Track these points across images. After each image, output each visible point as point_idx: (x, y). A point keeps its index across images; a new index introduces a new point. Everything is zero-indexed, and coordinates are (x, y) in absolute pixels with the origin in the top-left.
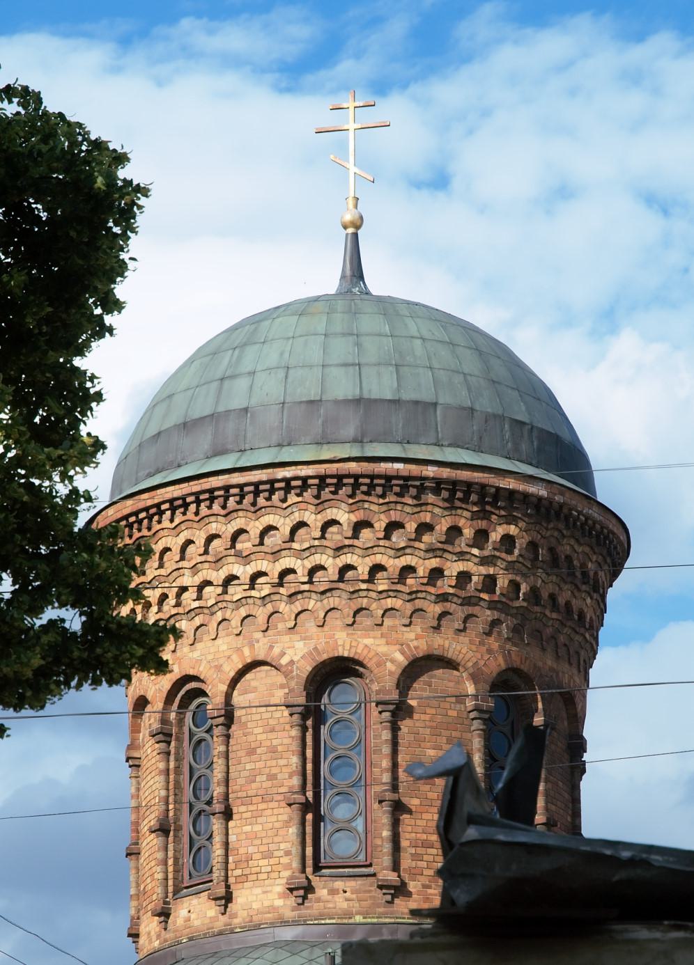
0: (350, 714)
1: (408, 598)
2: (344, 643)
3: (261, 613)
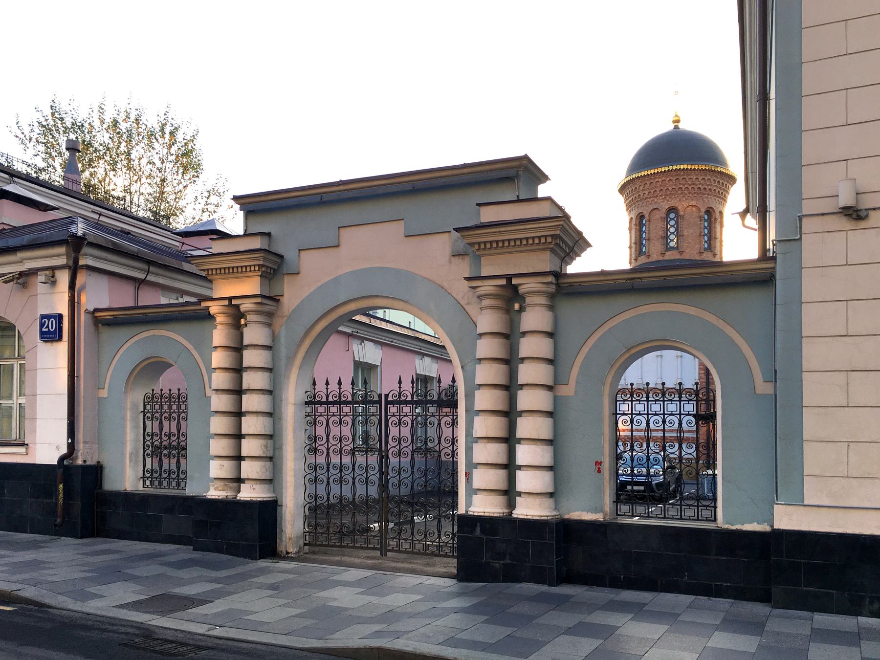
0: (171, 565)
3: (637, 205)
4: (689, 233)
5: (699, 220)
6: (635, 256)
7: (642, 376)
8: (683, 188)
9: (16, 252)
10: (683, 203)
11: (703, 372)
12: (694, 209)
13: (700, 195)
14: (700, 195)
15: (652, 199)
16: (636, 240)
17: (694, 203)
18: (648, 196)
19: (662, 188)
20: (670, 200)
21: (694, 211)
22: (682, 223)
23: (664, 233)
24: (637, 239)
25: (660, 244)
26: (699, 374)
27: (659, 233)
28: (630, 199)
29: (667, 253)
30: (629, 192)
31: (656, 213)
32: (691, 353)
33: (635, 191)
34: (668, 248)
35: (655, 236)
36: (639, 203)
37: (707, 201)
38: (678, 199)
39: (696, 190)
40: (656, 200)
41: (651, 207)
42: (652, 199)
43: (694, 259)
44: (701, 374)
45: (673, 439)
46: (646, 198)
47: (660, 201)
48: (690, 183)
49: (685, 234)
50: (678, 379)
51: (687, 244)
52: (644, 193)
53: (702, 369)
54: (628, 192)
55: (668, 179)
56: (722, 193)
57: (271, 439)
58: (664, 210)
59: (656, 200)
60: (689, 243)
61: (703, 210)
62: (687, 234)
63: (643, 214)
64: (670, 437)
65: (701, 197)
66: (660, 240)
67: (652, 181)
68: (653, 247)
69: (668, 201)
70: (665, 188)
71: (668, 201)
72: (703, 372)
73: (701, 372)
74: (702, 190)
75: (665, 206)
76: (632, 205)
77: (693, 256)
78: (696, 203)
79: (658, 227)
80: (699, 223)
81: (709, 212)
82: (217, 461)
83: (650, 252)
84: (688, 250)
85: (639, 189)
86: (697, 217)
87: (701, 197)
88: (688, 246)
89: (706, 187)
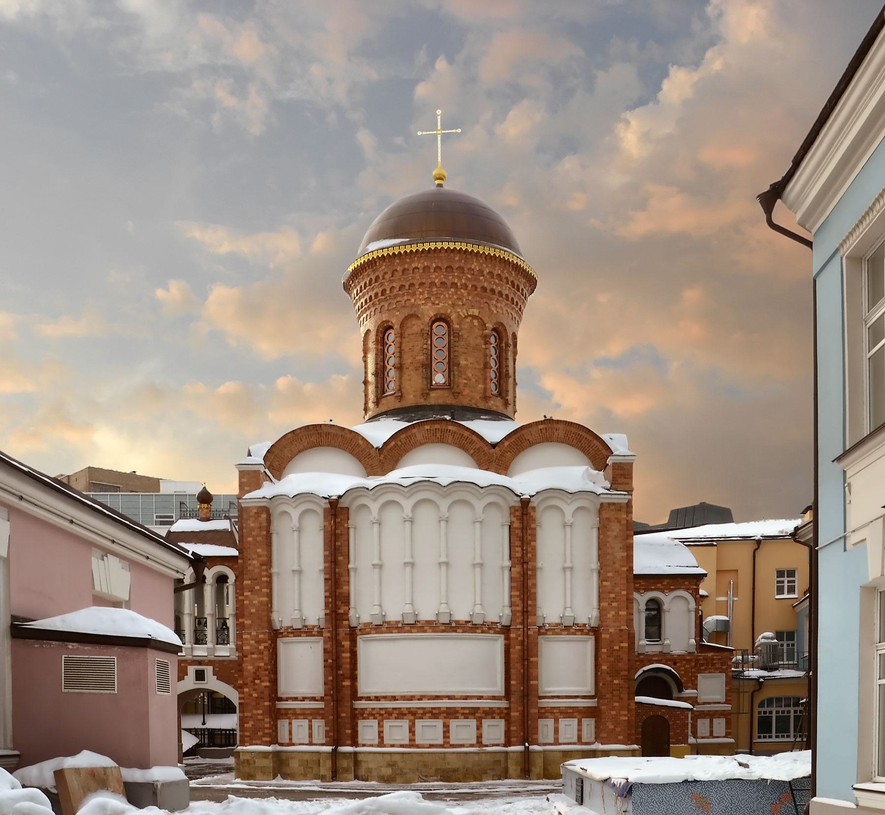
3: (378, 307)
4: (469, 363)
5: (483, 342)
6: (376, 396)
7: (412, 600)
8: (459, 284)
9: (357, 761)
10: (459, 310)
11: (518, 593)
12: (476, 322)
13: (485, 300)
14: (485, 300)
15: (406, 298)
16: (376, 368)
17: (476, 312)
18: (400, 292)
19: (424, 281)
20: (437, 302)
21: (475, 326)
22: (456, 344)
23: (427, 359)
24: (379, 367)
25: (420, 377)
26: (511, 597)
27: (418, 358)
28: (367, 297)
29: (433, 394)
30: (365, 284)
31: (413, 323)
32: (653, 530)
33: (365, 288)
34: (430, 387)
35: (412, 363)
36: (382, 304)
37: (495, 312)
38: (450, 303)
39: (479, 290)
40: (413, 300)
41: (406, 312)
42: (406, 298)
43: (475, 406)
44: (514, 596)
45: (467, 711)
46: (396, 296)
47: (419, 303)
48: (469, 276)
49: (461, 362)
50: (475, 605)
51: (466, 381)
52: (393, 287)
53: (514, 587)
54: (362, 284)
55: (434, 265)
56: (517, 302)
57: (622, 540)
58: (427, 319)
59: (413, 300)
60: (468, 379)
61: (490, 326)
62: (465, 363)
63: (390, 324)
64: (463, 708)
65: (486, 302)
66: (421, 369)
67: (406, 266)
68: (408, 382)
69: (433, 304)
70: (429, 281)
71: (433, 304)
72: (518, 593)
73: (513, 593)
74: (488, 291)
75: (429, 311)
76: (369, 308)
77: (473, 401)
78: (479, 312)
79: (418, 348)
80: (483, 346)
81: (499, 331)
83: (403, 390)
84: (466, 391)
85: (383, 278)
86: (481, 336)
87: (486, 302)
88: (465, 384)
89: (495, 287)
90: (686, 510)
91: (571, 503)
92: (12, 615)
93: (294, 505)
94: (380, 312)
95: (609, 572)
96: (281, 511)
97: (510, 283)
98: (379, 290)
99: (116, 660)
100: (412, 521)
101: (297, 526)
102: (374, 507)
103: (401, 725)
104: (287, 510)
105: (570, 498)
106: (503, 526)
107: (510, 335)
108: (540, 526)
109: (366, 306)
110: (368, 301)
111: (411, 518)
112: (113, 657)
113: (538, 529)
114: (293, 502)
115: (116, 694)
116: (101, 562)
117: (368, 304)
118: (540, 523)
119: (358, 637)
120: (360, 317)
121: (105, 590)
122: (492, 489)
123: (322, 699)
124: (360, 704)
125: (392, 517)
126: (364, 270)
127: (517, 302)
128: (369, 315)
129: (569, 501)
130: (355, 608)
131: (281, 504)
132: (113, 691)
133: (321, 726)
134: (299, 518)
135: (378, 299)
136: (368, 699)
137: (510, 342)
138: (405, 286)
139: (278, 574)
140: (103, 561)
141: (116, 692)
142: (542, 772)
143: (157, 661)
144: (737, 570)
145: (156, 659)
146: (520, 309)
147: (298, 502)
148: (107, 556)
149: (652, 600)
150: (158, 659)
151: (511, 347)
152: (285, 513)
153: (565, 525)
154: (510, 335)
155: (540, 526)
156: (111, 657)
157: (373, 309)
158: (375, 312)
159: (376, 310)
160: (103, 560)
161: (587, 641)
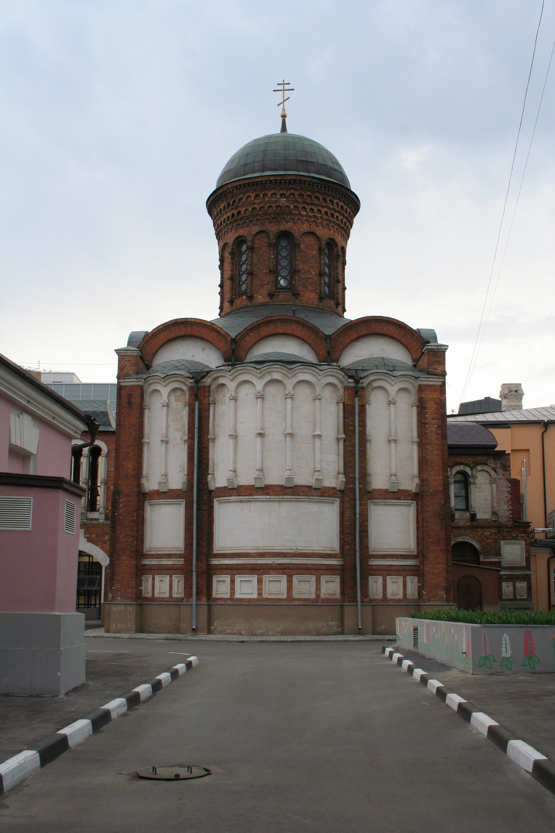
1: (258, 204)
2: (241, 232)
54: (222, 207)
82: (487, 733)
90: (467, 405)
91: (395, 384)
92: (115, 350)
93: (164, 384)
94: (235, 230)
95: (427, 445)
96: (153, 389)
97: (340, 208)
98: (235, 212)
99: (32, 500)
100: (262, 397)
101: (87, 454)
102: (231, 386)
103: (250, 580)
104: (158, 389)
105: (393, 380)
106: (338, 403)
107: (339, 249)
108: (369, 404)
109: (228, 222)
110: (226, 221)
111: (262, 395)
112: (30, 498)
113: (367, 406)
114: (164, 382)
115: (30, 531)
116: (17, 419)
117: (226, 223)
118: (369, 401)
119: (215, 500)
120: (219, 233)
121: (19, 444)
122: (331, 371)
123: (180, 556)
124: (215, 562)
125: (246, 393)
126: (220, 199)
127: (345, 222)
128: (226, 232)
129: (393, 383)
130: (213, 474)
131: (154, 383)
132: (28, 529)
133: (180, 581)
134: (168, 395)
135: (235, 219)
136: (224, 556)
137: (340, 253)
138: (256, 208)
139: (148, 443)
140: (19, 419)
141: (30, 530)
142: (481, 548)
143: (67, 502)
144: (528, 450)
145: (66, 500)
146: (348, 228)
147: (168, 382)
148: (22, 414)
149: (459, 472)
150: (68, 501)
151: (341, 258)
152: (157, 391)
153: (390, 403)
154: (339, 249)
155: (369, 404)
156: (29, 498)
157: (230, 227)
158: (231, 229)
159: (233, 228)
160: (19, 417)
161: (410, 505)
